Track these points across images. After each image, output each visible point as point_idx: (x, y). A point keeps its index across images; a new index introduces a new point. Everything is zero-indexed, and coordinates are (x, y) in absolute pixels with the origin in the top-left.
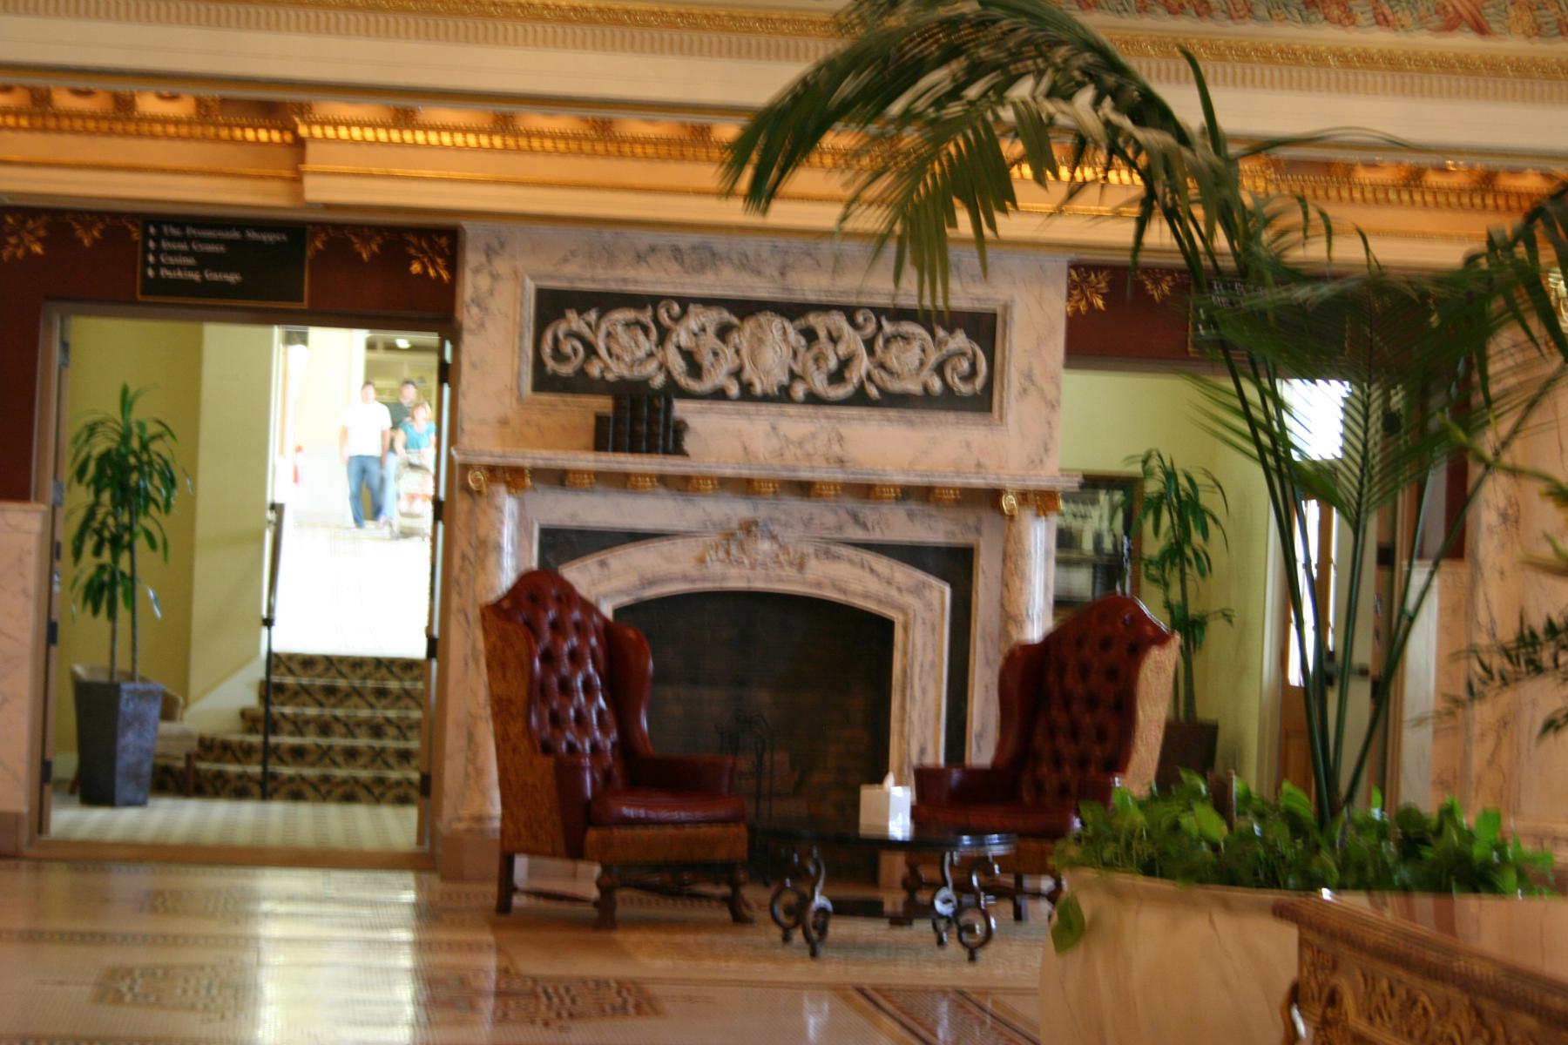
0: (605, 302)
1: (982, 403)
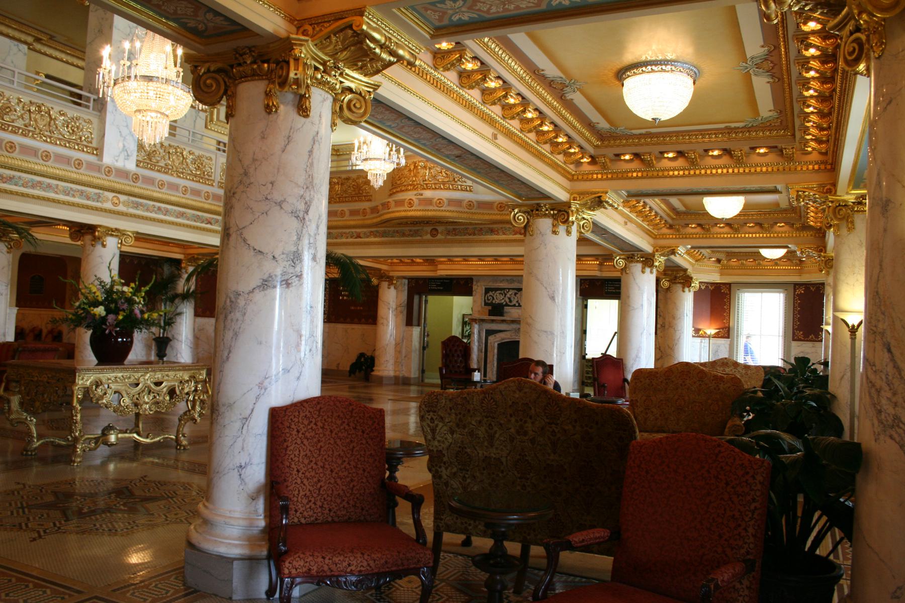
0: (496, 290)
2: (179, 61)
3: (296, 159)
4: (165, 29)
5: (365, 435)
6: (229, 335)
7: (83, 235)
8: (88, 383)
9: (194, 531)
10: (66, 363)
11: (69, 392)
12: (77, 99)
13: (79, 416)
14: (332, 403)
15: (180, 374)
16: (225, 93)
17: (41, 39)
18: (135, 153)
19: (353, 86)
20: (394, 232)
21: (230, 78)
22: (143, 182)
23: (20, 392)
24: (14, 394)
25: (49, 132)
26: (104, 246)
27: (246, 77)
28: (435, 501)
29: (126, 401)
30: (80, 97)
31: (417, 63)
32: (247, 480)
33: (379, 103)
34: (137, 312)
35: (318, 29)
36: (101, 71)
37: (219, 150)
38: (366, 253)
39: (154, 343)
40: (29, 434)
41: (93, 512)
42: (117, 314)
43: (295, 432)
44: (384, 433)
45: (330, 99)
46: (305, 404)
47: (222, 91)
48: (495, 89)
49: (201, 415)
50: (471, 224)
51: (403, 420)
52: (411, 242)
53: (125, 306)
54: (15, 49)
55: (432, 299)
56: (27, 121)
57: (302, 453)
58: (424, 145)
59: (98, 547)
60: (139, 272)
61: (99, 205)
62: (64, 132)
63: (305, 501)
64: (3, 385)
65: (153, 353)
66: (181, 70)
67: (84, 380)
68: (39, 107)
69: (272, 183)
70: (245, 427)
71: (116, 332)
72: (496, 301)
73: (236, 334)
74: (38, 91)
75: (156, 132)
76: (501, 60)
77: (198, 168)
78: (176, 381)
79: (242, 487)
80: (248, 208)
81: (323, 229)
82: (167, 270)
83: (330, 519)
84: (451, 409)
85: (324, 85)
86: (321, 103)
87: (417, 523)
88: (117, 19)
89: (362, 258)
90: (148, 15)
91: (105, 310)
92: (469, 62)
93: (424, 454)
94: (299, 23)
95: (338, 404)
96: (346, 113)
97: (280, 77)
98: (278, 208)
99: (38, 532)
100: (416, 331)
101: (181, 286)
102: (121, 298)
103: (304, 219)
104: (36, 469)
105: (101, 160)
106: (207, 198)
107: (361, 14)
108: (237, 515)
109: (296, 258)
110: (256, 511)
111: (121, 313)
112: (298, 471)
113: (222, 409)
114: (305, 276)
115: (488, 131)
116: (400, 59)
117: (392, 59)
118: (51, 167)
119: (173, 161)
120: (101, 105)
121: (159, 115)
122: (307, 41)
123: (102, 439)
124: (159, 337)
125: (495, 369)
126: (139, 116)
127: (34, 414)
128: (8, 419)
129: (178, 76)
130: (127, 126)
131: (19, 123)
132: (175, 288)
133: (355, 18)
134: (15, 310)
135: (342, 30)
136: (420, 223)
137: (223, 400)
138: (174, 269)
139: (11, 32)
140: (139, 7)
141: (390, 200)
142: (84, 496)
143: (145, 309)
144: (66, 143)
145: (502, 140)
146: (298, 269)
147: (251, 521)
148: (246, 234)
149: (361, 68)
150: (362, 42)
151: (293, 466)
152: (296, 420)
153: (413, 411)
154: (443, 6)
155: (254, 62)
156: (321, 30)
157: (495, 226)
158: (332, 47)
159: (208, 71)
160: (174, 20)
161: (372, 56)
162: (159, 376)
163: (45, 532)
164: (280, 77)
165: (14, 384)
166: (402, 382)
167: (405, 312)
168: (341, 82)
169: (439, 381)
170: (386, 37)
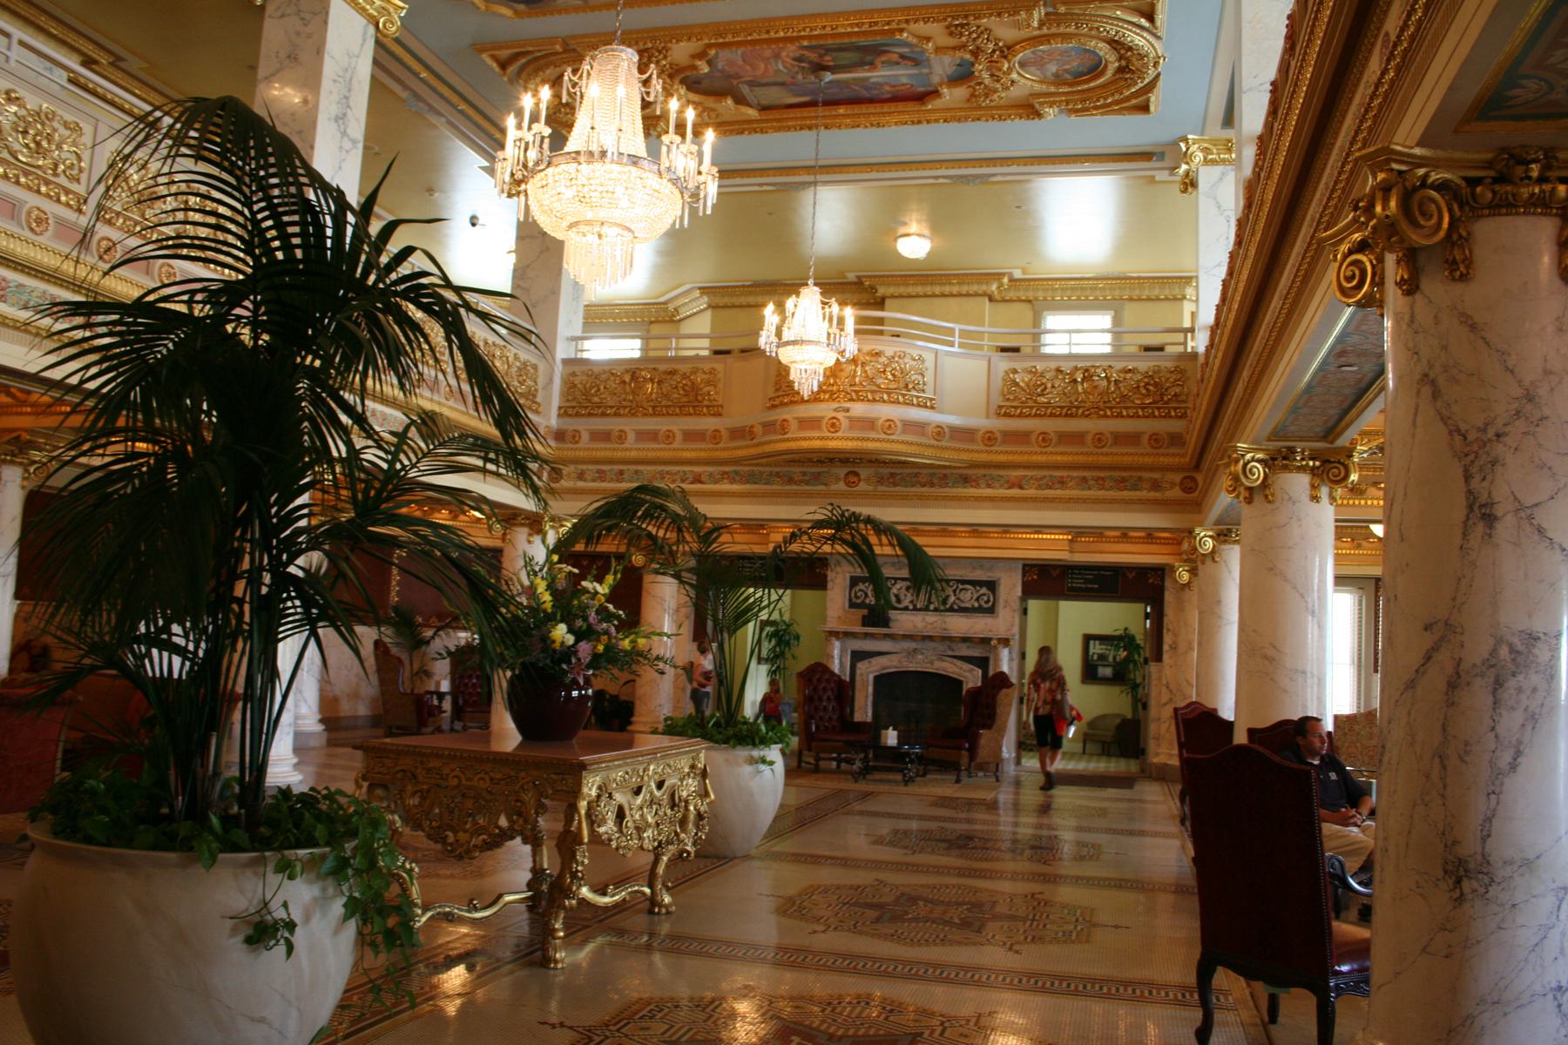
1: (991, 611)
6: (1510, 722)
17: (96, 62)
20: (771, 474)
62: (16, 147)
80: (1542, 466)
148: (1541, 517)
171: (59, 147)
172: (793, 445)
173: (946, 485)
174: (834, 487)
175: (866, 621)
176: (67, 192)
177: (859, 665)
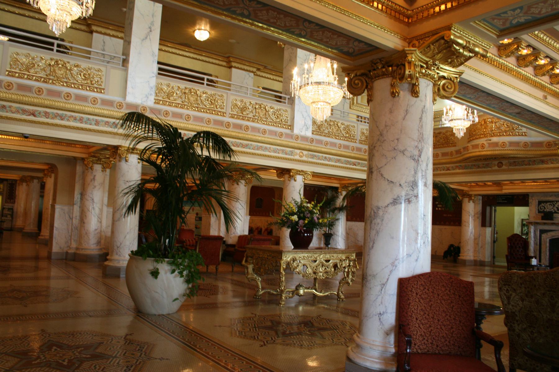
0: (546, 202)
2: (335, 71)
3: (412, 124)
4: (330, 54)
5: (461, 299)
6: (373, 233)
7: (284, 174)
8: (289, 259)
9: (350, 351)
10: (274, 247)
11: (278, 264)
12: (279, 99)
13: (284, 278)
14: (438, 277)
15: (340, 256)
16: (367, 87)
18: (311, 127)
19: (445, 75)
20: (472, 165)
21: (369, 78)
22: (301, 140)
23: (253, 263)
24: (250, 264)
25: (265, 119)
26: (295, 180)
27: (378, 76)
28: (510, 346)
29: (310, 270)
30: (280, 97)
31: (488, 55)
32: (384, 323)
33: (463, 84)
34: (316, 218)
35: (422, 42)
36: (293, 82)
37: (358, 121)
38: (455, 180)
39: (323, 237)
40: (257, 287)
41: (291, 334)
42: (304, 220)
43: (414, 294)
44: (474, 298)
45: (431, 85)
46: (421, 277)
47: (364, 86)
48: (544, 65)
49: (352, 280)
50: (526, 158)
51: (486, 290)
52: (485, 172)
53: (309, 215)
54: (248, 76)
55: (499, 209)
56: (254, 114)
57: (419, 308)
58: (494, 107)
59: (294, 354)
60: (316, 195)
61: (292, 157)
62: (206, 104)
63: (421, 339)
64: (245, 259)
65: (323, 242)
66: (337, 76)
67: (287, 258)
68: (260, 105)
69: (398, 139)
70: (383, 290)
71: (304, 230)
72: (547, 210)
73: (377, 232)
74: (259, 97)
75: (323, 114)
76: (548, 45)
77: (347, 133)
78: (338, 259)
79: (380, 327)
80: (383, 155)
81: (431, 166)
82: (330, 193)
83: (437, 352)
84: (521, 284)
85: (427, 76)
86: (426, 87)
87: (499, 361)
88: (299, 51)
89: (451, 183)
90: (321, 48)
91: (298, 217)
92: (524, 49)
93: (501, 313)
94: (410, 41)
95: (442, 277)
96: (442, 92)
97: (400, 74)
98: (402, 154)
99: (264, 342)
100: (488, 230)
101: (339, 202)
102: (306, 211)
103: (418, 160)
104: (261, 306)
105: (293, 131)
106: (353, 150)
107: (450, 29)
108: (377, 343)
109: (414, 185)
110: (389, 342)
111: (307, 219)
112: (417, 319)
113: (369, 278)
114: (420, 196)
115: (540, 94)
116: (476, 54)
117: (471, 54)
118: (267, 138)
119: (333, 129)
120: (292, 101)
121: (325, 104)
122: (415, 50)
123: (296, 292)
124: (326, 233)
125: (548, 257)
126: (314, 105)
127: (260, 275)
128: (247, 278)
129: (335, 80)
130: (306, 111)
131: (251, 115)
132: (335, 204)
133: (445, 32)
134: (249, 217)
135: (437, 41)
136: (490, 159)
137: (369, 272)
138: (334, 193)
139: (246, 67)
140: (316, 44)
141: (469, 145)
142: (287, 324)
143: (320, 217)
144: (274, 124)
145: (550, 99)
146: (415, 192)
147: (385, 347)
148: (384, 171)
149: (451, 63)
150: (451, 46)
151: (413, 315)
152: (415, 286)
153: (487, 283)
154: (505, 15)
155: (383, 67)
156: (424, 43)
157: (545, 158)
158: (431, 52)
159: (356, 75)
160: (336, 49)
161: (457, 54)
162: (328, 256)
163: (267, 342)
164: (400, 74)
165: (250, 258)
166: (479, 264)
167: (480, 218)
168: (438, 73)
169: (506, 264)
170: (466, 41)
171: (217, 102)
172: (471, 155)
173: (535, 164)
174: (494, 168)
175: (543, 218)
176: (220, 112)
177: (543, 235)
